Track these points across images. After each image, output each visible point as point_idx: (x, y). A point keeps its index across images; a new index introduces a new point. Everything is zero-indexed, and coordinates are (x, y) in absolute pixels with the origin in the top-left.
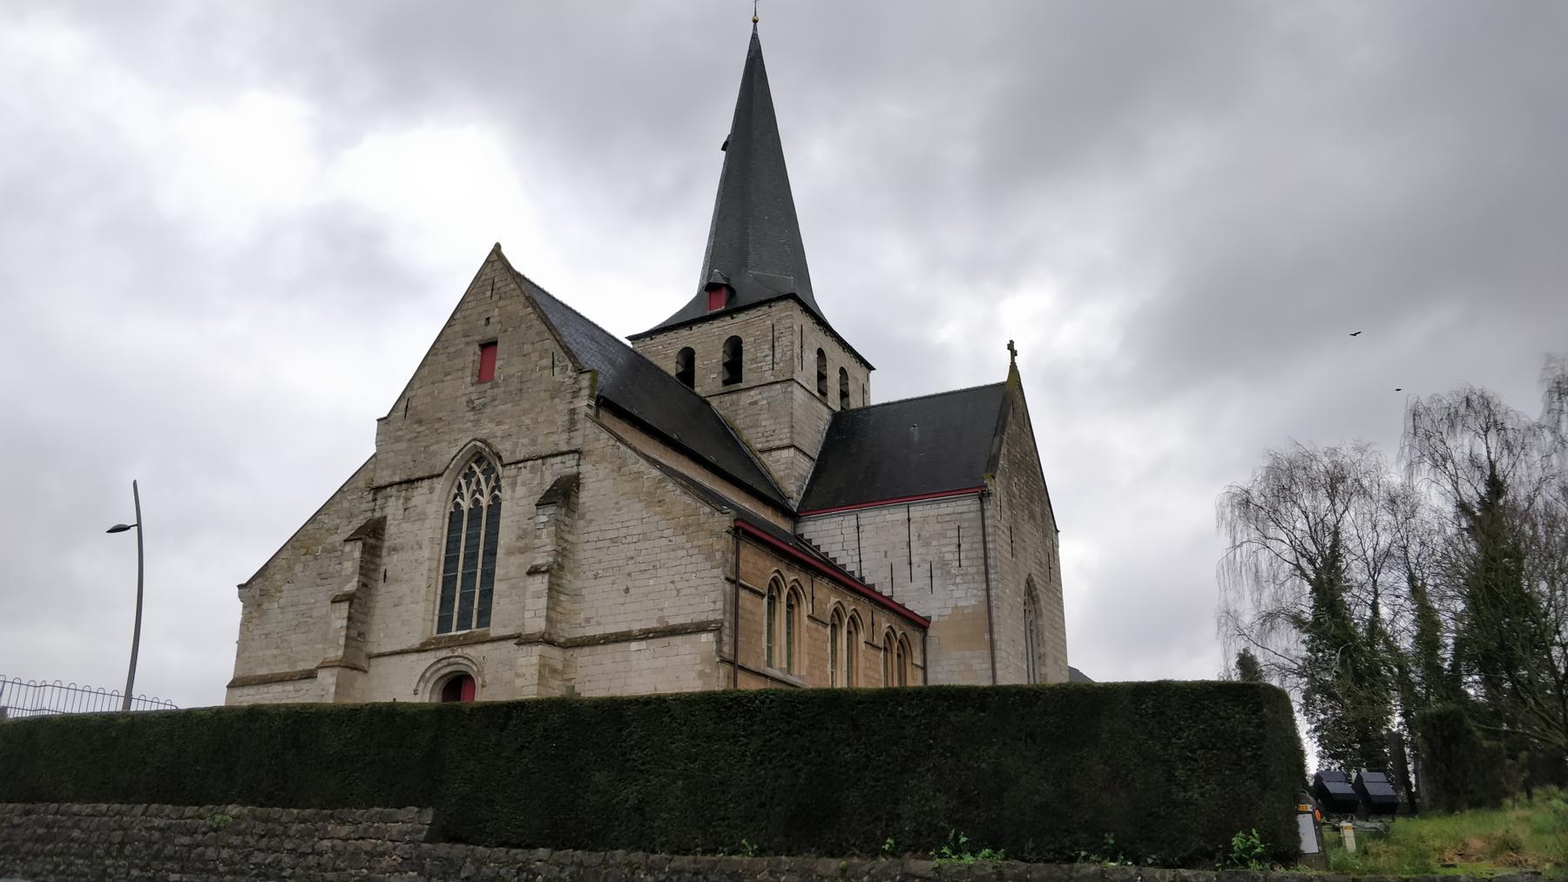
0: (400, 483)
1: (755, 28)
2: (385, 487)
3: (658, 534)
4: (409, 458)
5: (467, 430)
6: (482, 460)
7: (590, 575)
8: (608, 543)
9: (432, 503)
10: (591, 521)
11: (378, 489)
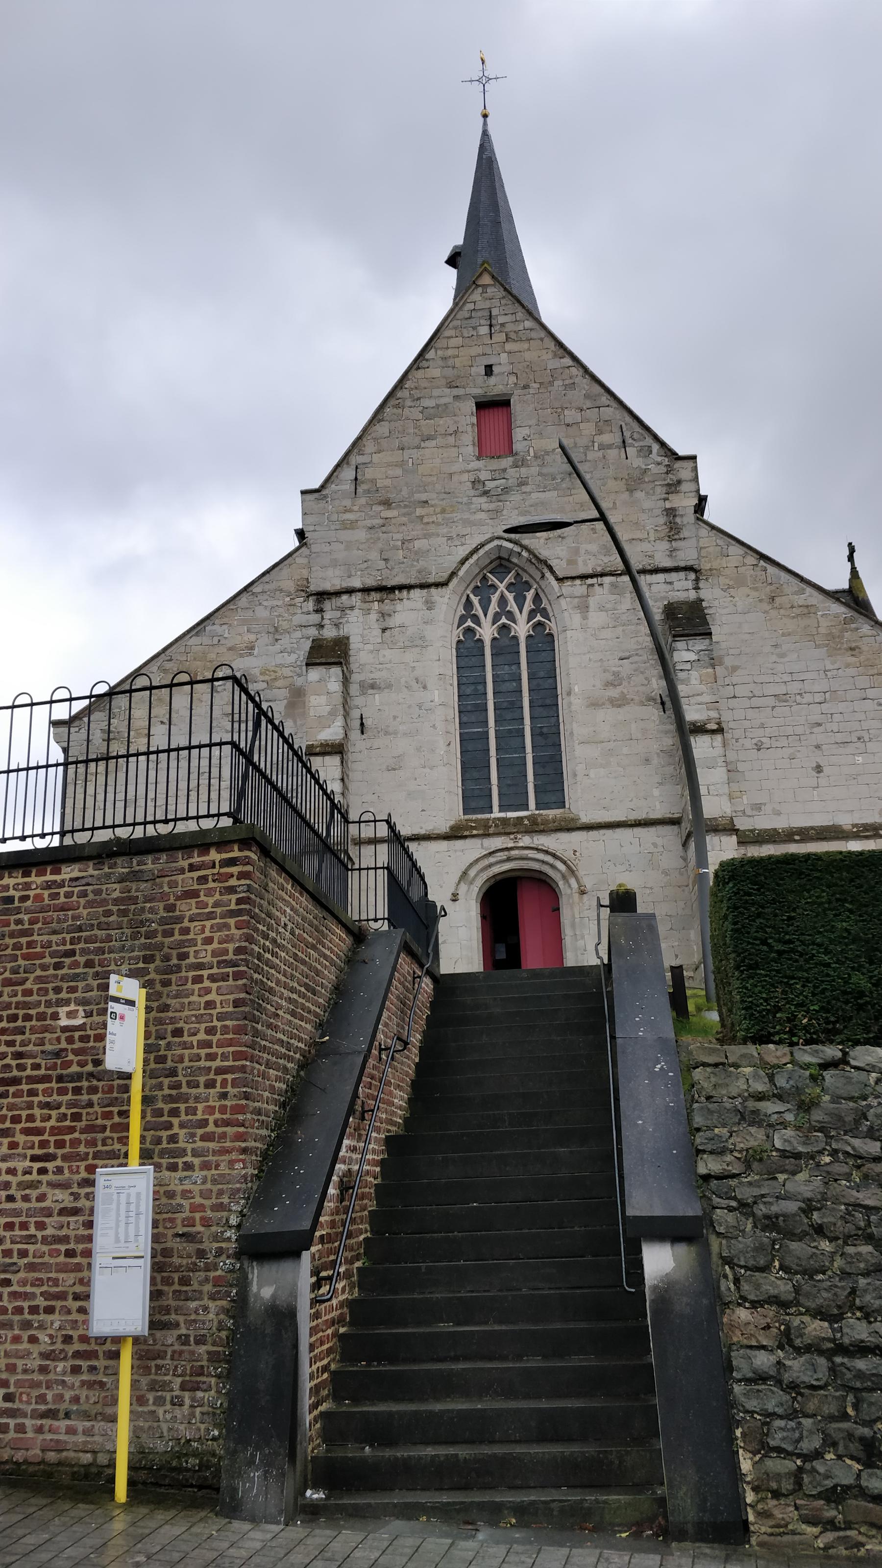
0: (366, 590)
1: (485, 124)
2: (338, 594)
3: (859, 694)
4: (374, 555)
5: (481, 523)
6: (508, 567)
7: (748, 744)
8: (771, 701)
9: (430, 629)
10: (735, 669)
11: (322, 596)
